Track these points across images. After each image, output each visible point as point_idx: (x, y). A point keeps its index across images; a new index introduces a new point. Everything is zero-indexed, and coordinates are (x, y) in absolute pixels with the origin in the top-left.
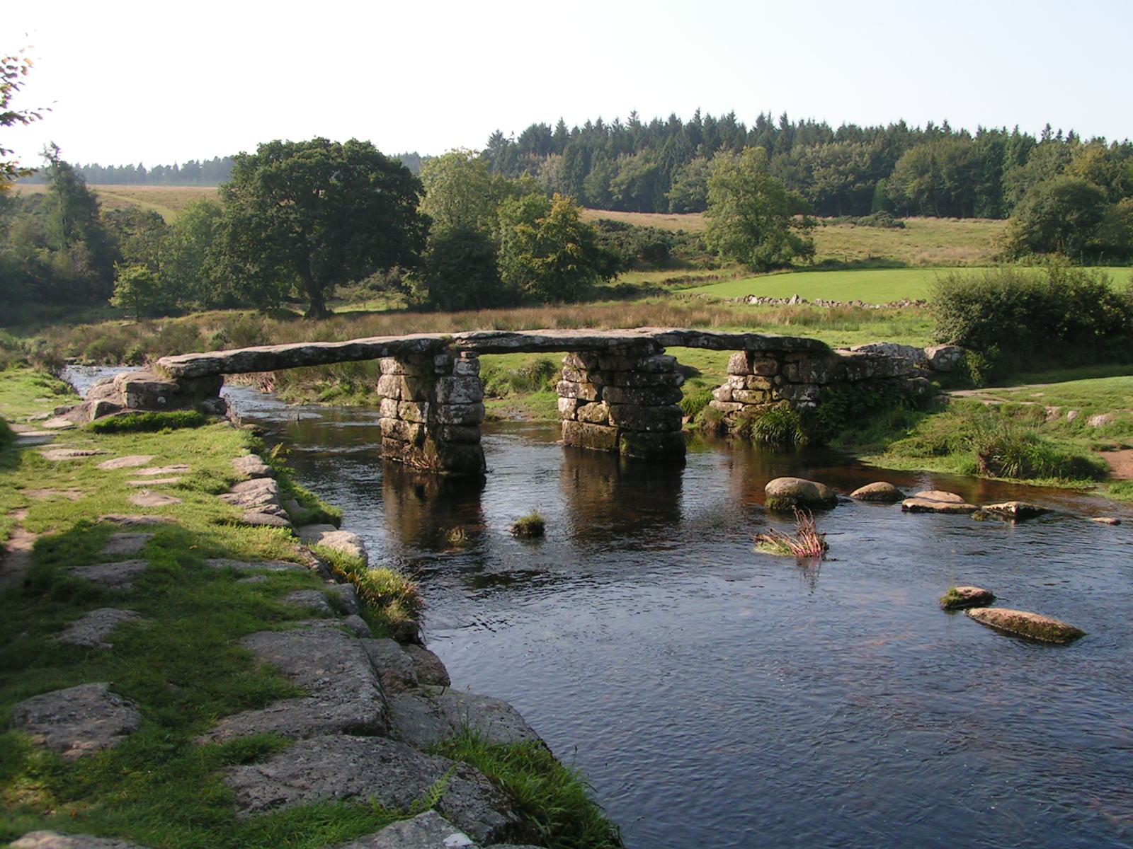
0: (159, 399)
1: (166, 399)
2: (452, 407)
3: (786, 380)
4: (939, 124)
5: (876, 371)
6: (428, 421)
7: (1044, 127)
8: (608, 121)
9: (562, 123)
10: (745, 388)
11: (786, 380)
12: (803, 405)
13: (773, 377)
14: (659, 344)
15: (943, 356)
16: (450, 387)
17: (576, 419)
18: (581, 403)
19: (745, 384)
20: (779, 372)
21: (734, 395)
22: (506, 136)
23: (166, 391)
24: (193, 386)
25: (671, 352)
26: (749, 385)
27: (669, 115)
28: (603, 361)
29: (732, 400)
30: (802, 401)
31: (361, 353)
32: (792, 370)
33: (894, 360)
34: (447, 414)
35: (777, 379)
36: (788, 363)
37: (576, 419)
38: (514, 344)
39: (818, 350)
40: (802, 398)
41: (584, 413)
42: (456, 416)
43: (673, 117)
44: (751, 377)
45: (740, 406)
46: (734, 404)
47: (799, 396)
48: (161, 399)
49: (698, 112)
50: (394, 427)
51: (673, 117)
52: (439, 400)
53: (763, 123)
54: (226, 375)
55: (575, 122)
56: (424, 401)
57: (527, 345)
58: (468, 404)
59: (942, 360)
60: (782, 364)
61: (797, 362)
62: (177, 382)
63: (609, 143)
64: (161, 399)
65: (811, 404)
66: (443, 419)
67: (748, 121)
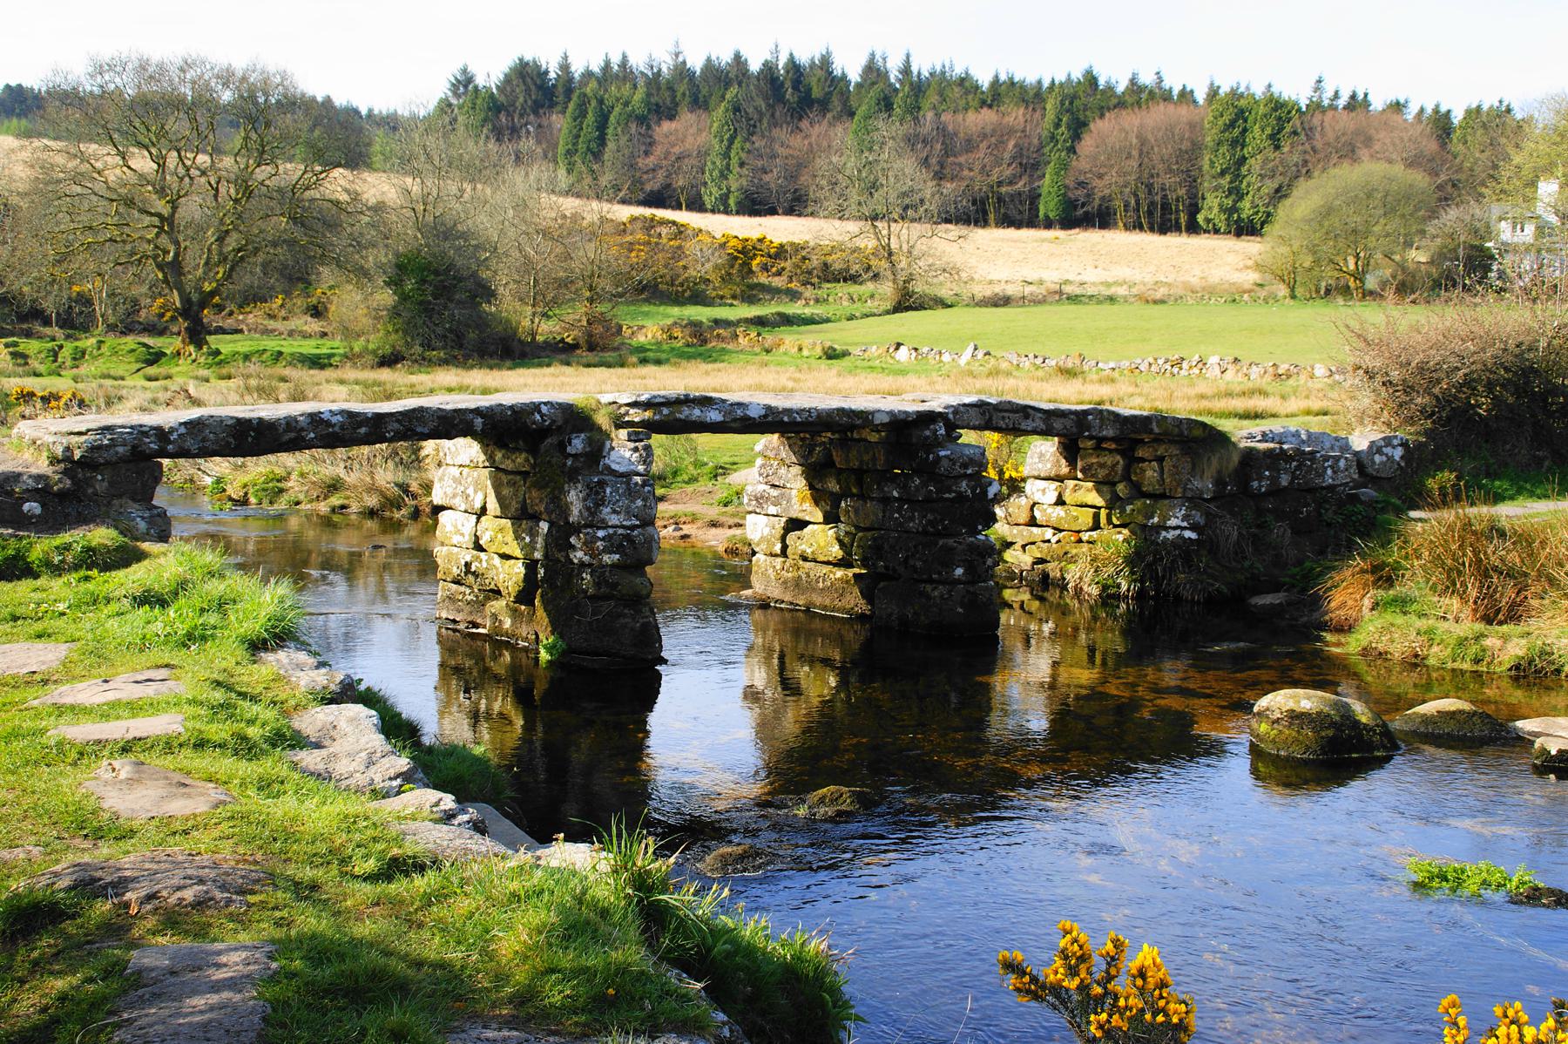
0: (26, 507)
1: (43, 506)
2: (601, 534)
3: (1138, 492)
4: (1147, 79)
5: (1294, 477)
6: (546, 556)
7: (1312, 83)
8: (638, 62)
9: (1437, 106)
10: (1060, 502)
11: (1138, 492)
12: (1171, 535)
13: (1114, 484)
14: (952, 421)
15: (1379, 451)
16: (595, 497)
17: (784, 553)
18: (795, 525)
19: (1060, 496)
20: (1126, 477)
21: (1037, 514)
22: (480, 81)
23: (42, 490)
24: (100, 483)
25: (968, 437)
26: (1067, 498)
27: (863, 61)
28: (840, 452)
29: (1032, 522)
30: (1167, 529)
31: (432, 425)
32: (1150, 473)
33: (1327, 458)
34: (589, 545)
35: (1121, 488)
36: (1143, 460)
37: (784, 553)
38: (714, 416)
39: (1218, 439)
40: (1169, 523)
41: (803, 542)
42: (606, 550)
43: (737, 57)
44: (1071, 483)
45: (1048, 534)
46: (1035, 530)
47: (1165, 518)
48: (32, 507)
49: (908, 56)
50: (467, 565)
51: (737, 57)
52: (574, 517)
53: (873, 71)
54: (166, 462)
55: (586, 59)
56: (536, 518)
57: (735, 420)
58: (633, 528)
59: (1377, 458)
60: (1132, 461)
61: (1160, 460)
62: (65, 472)
63: (639, 95)
64: (32, 507)
65: (1188, 534)
66: (580, 554)
67: (850, 67)
